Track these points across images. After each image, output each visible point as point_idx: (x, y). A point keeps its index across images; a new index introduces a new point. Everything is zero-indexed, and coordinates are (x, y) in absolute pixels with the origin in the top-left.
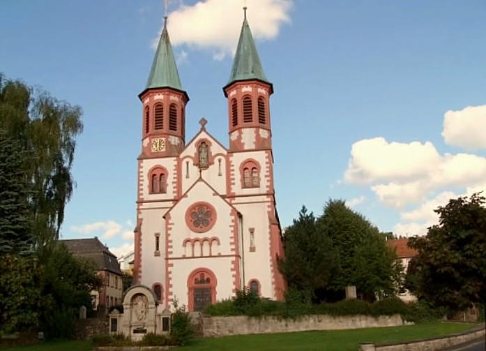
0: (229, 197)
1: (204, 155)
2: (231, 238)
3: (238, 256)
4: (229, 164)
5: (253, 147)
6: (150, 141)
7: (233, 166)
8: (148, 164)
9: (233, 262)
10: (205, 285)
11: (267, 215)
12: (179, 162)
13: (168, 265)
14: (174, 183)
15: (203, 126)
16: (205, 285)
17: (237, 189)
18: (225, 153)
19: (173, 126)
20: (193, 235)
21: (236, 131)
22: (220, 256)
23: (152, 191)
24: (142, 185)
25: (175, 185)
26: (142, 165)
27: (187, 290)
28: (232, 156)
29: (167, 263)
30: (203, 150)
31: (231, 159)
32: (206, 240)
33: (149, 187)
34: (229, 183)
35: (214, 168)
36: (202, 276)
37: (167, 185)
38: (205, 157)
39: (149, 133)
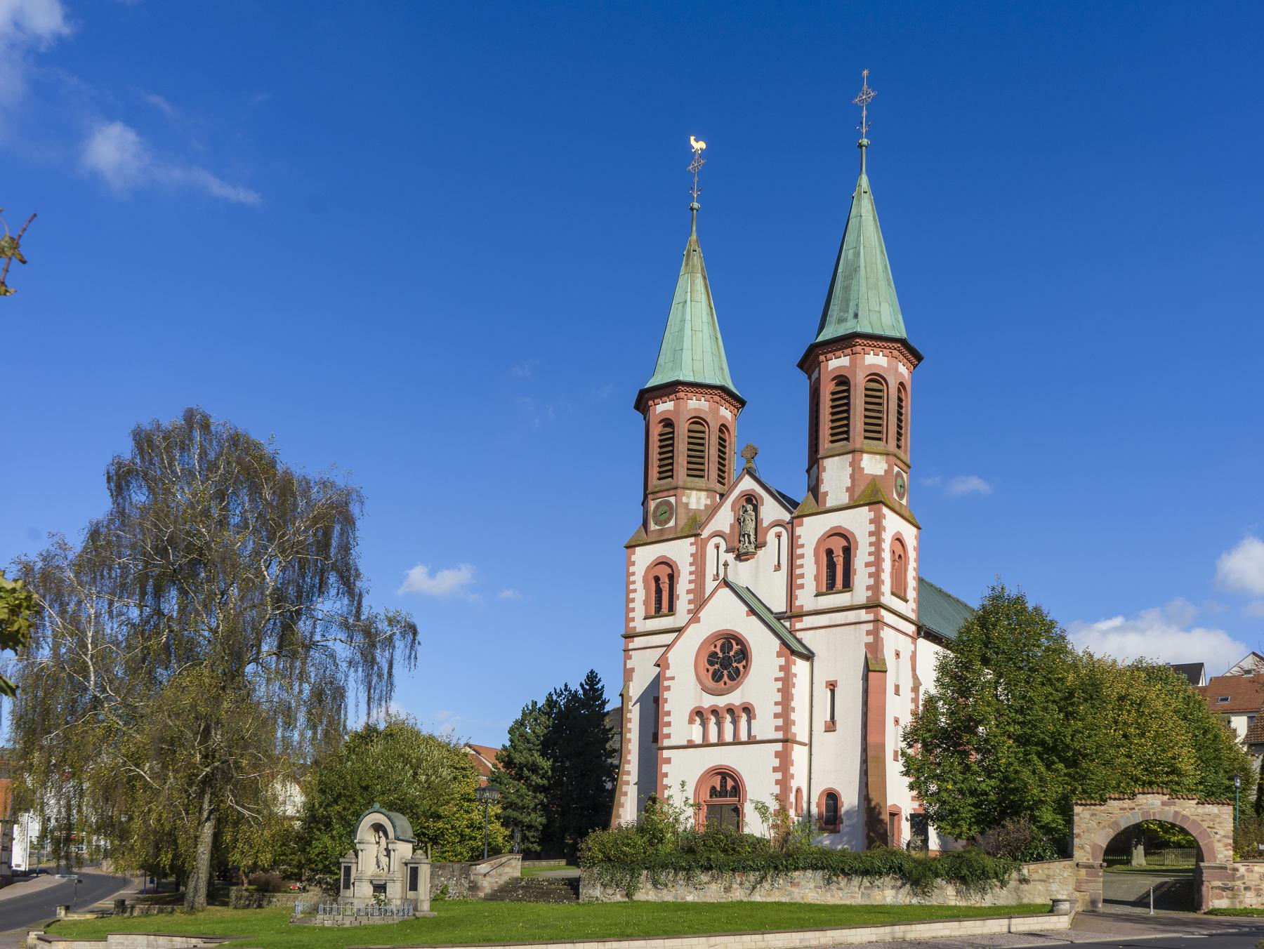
2: (776, 704)
7: (802, 546)
9: (777, 754)
14: (689, 592)
17: (806, 598)
20: (708, 701)
28: (801, 525)
34: (792, 587)
35: (767, 556)
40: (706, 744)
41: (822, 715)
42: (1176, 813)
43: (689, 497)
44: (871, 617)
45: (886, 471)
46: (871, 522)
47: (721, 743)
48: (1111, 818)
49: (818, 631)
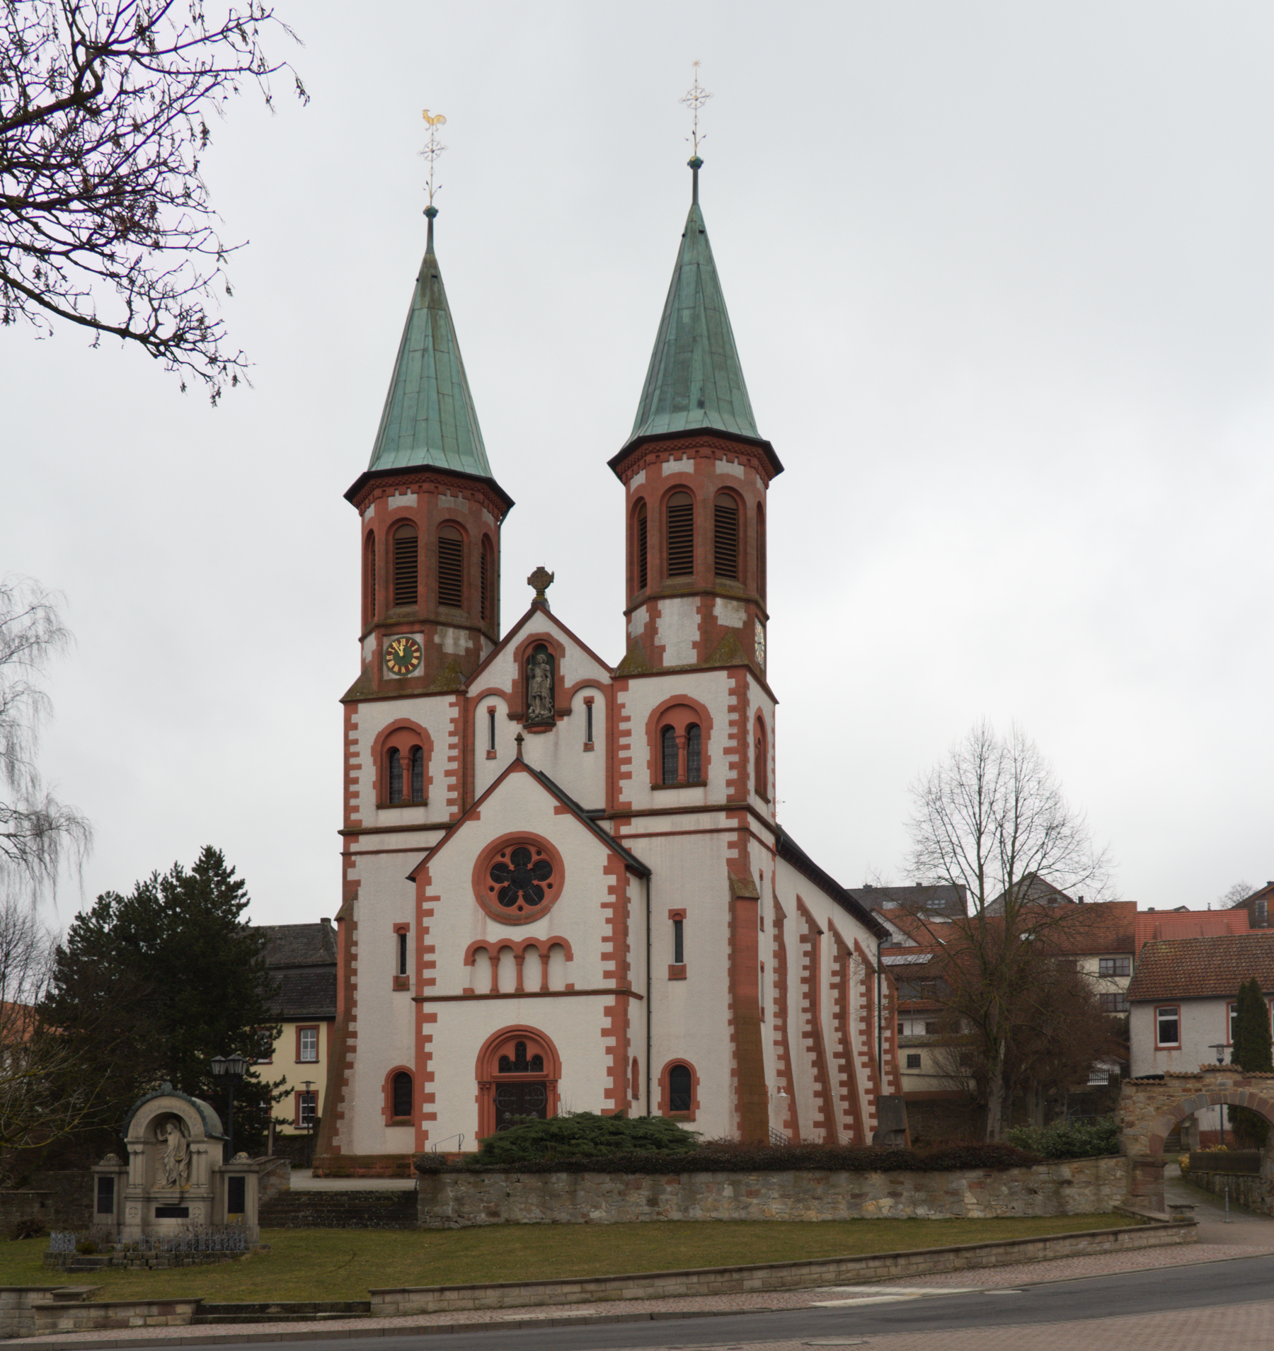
0: (611, 818)
1: (539, 682)
2: (605, 939)
3: (624, 993)
4: (614, 713)
5: (691, 657)
6: (380, 644)
7: (628, 719)
8: (378, 716)
9: (608, 1011)
10: (529, 1075)
11: (724, 870)
12: (467, 708)
13: (423, 1018)
14: (448, 773)
15: (541, 592)
16: (529, 1075)
18: (605, 678)
19: (450, 594)
20: (496, 932)
21: (644, 608)
22: (570, 992)
23: (663, 780)
24: (356, 781)
25: (453, 780)
26: (354, 718)
27: (473, 1089)
29: (419, 1011)
30: (538, 672)
31: (621, 697)
32: (530, 945)
33: (650, 765)
34: (614, 774)
35: (570, 728)
36: (521, 1048)
37: (430, 780)
38: (545, 693)
39: (648, 591)
40: (495, 995)
41: (663, 956)
42: (1252, 1095)
43: (443, 636)
44: (734, 823)
45: (745, 623)
46: (732, 692)
47: (520, 994)
48: (1173, 1102)
49: (654, 839)
